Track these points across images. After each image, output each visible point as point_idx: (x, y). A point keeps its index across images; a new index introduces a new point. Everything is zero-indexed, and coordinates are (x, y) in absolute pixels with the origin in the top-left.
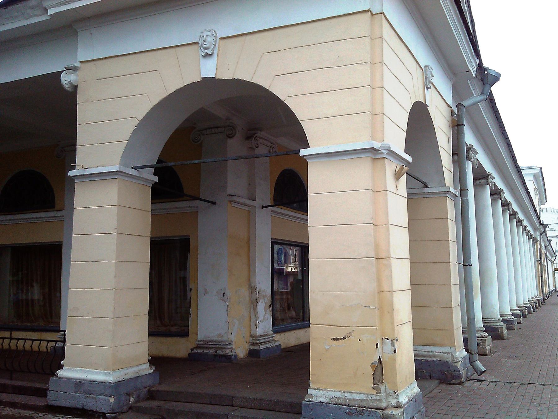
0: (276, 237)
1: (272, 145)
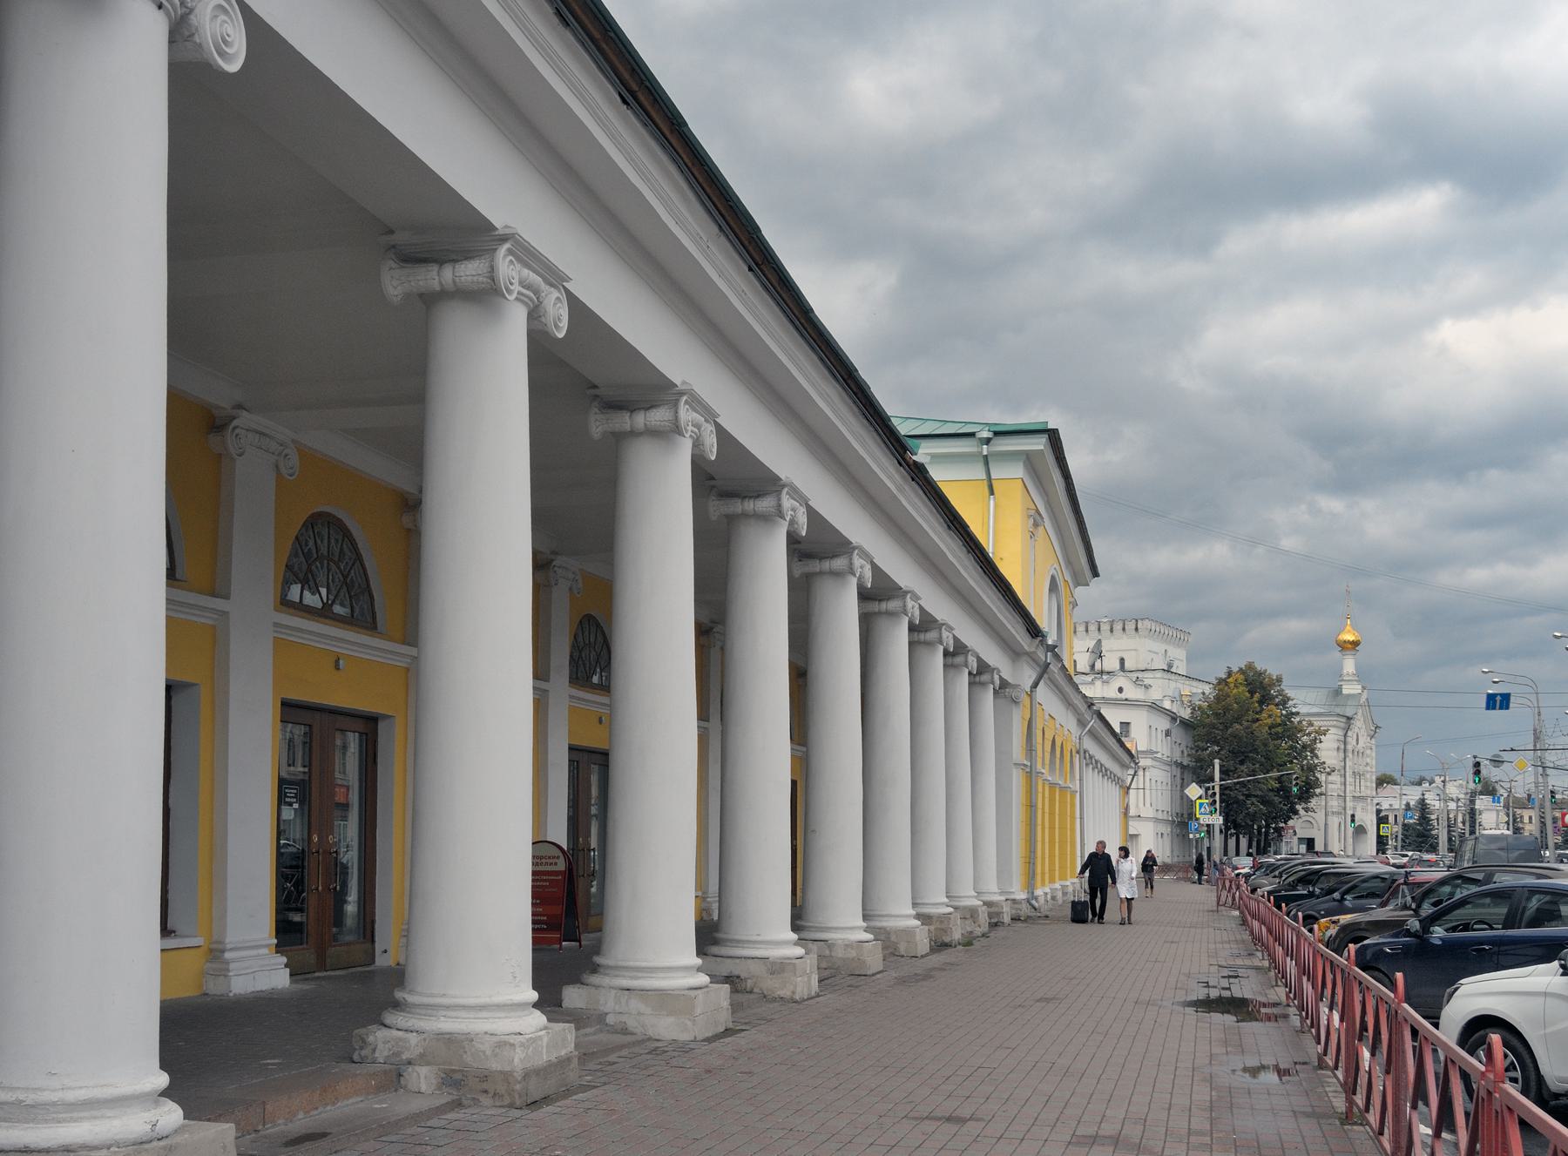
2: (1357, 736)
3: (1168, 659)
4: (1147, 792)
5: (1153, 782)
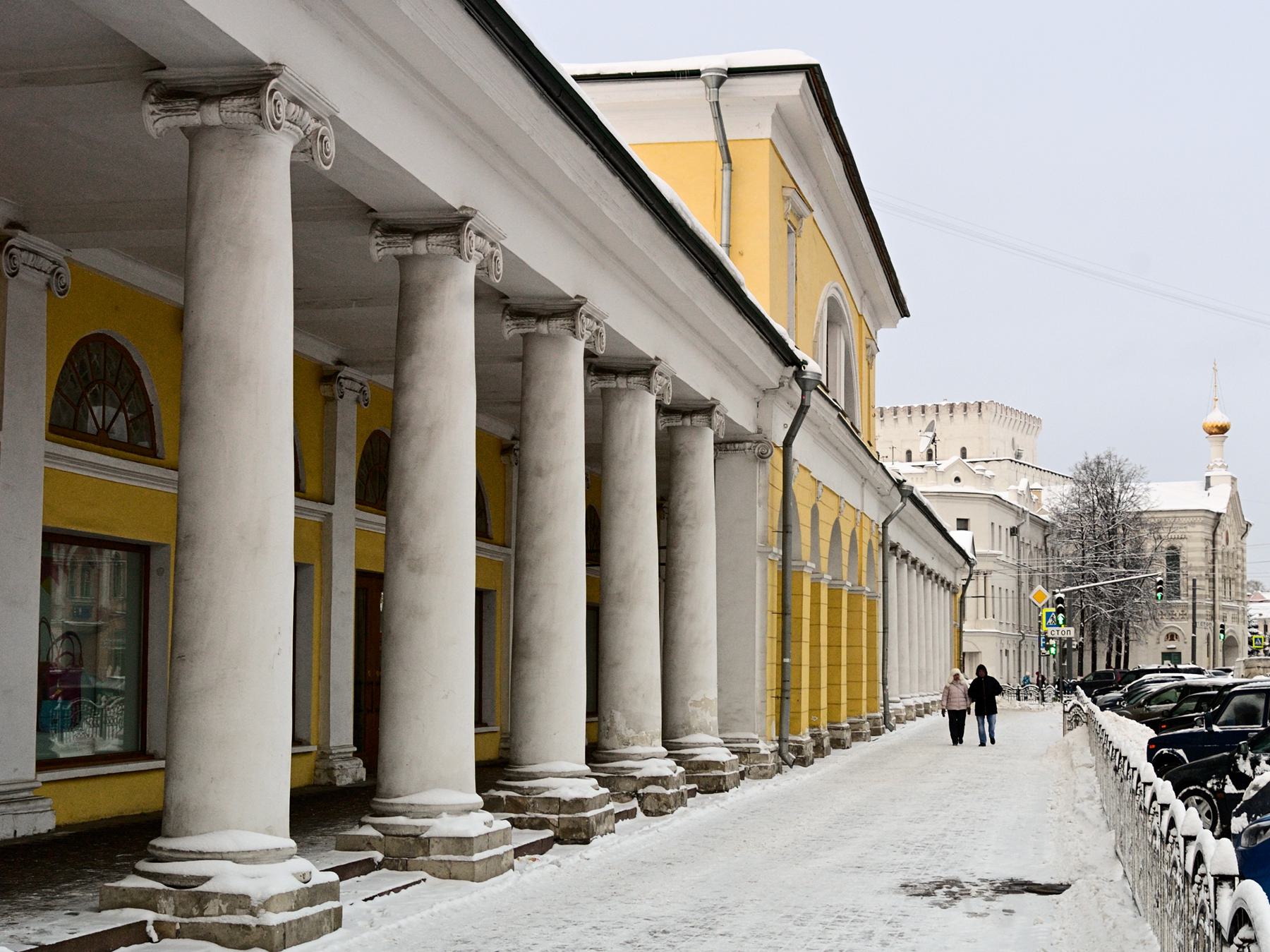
0: (50, 525)
1: (56, 268)
2: (1227, 534)
3: (1016, 449)
4: (989, 600)
5: (1003, 592)
